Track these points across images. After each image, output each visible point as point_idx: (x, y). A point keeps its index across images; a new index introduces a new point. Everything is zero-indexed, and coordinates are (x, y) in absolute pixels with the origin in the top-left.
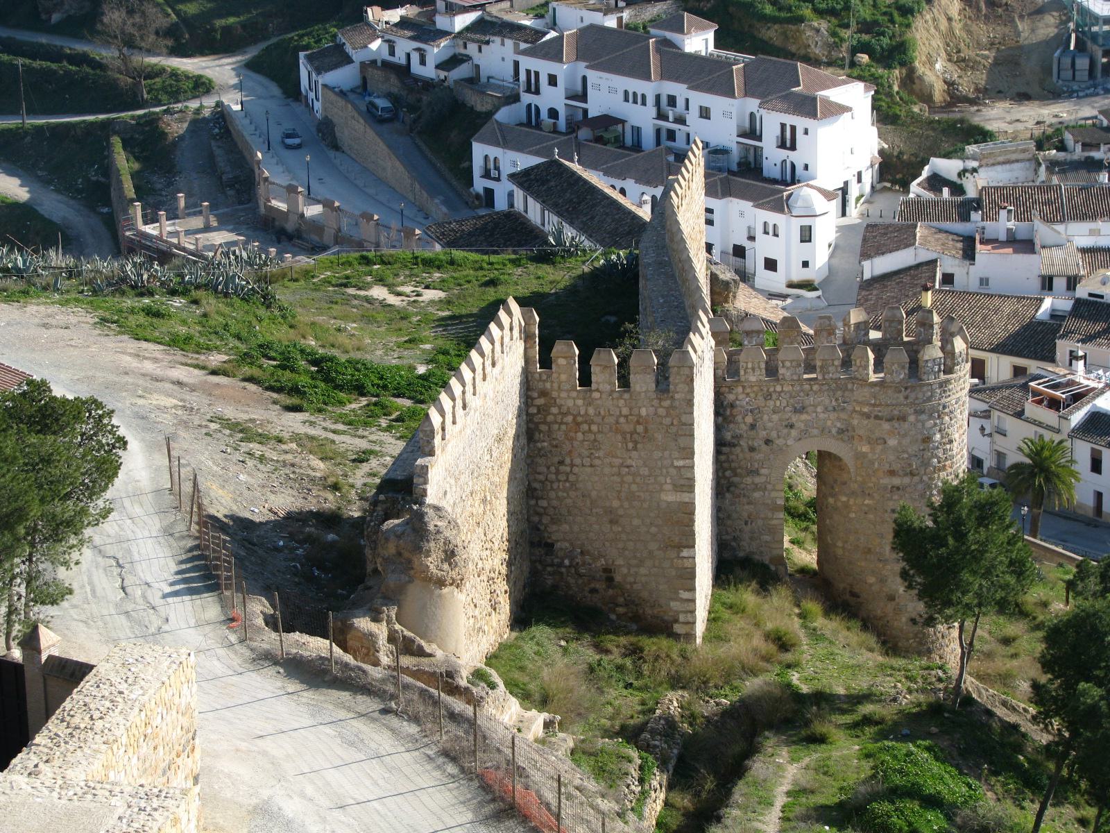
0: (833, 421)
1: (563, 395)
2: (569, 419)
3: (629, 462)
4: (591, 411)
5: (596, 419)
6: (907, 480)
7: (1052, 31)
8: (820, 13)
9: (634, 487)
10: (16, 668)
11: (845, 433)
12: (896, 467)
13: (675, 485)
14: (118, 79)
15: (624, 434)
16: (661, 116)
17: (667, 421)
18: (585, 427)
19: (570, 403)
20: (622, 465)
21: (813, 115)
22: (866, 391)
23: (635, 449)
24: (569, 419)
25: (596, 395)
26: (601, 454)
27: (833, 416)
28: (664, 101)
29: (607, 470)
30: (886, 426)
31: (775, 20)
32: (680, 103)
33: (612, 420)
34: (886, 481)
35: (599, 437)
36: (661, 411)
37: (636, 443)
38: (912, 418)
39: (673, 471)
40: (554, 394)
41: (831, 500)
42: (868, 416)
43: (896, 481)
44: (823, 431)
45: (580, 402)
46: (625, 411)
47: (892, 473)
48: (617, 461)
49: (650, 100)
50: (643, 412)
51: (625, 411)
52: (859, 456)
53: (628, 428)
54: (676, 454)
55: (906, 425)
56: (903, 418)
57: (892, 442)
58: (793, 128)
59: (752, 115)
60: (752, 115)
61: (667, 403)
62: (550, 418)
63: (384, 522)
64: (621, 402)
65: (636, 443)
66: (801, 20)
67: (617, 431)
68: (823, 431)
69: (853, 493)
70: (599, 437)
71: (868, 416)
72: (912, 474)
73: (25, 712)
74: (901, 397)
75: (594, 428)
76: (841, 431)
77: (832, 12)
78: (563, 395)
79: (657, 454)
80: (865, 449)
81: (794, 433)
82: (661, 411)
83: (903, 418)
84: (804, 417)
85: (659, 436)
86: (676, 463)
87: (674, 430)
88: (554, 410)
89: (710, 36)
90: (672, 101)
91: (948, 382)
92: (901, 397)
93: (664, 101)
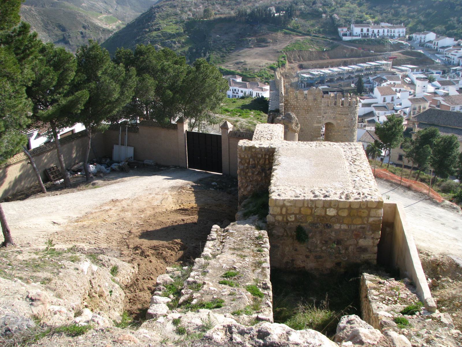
0: (332, 116)
1: (291, 101)
2: (293, 107)
3: (306, 117)
4: (298, 105)
5: (299, 107)
6: (348, 128)
7: (297, 80)
8: (258, 76)
9: (307, 123)
10: (217, 138)
11: (334, 118)
12: (346, 125)
13: (317, 122)
14: (161, 46)
15: (305, 110)
16: (233, 93)
17: (315, 106)
18: (296, 108)
19: (293, 103)
20: (305, 118)
21: (262, 90)
22: (340, 109)
23: (308, 113)
24: (293, 107)
25: (299, 101)
26: (300, 115)
27: (332, 114)
28: (234, 90)
29: (301, 119)
30: (344, 116)
31: (250, 78)
32: (237, 90)
33: (303, 107)
34: (343, 129)
35: (299, 111)
36: (314, 104)
37: (308, 112)
38: (349, 114)
39: (317, 119)
40: (289, 101)
41: (330, 134)
42: (340, 114)
43: (346, 129)
44: (330, 118)
45: (295, 102)
46: (306, 104)
47: (345, 127)
48: (304, 117)
49: (231, 90)
50: (310, 104)
51: (306, 104)
52: (337, 123)
53: (306, 108)
54: (317, 115)
55: (348, 116)
56: (347, 115)
57: (345, 120)
58: (259, 93)
59: (251, 92)
60: (251, 92)
61: (316, 102)
62: (288, 106)
63: (242, 138)
64: (305, 102)
65: (308, 112)
66: (255, 77)
67: (304, 109)
68: (330, 118)
69: (336, 132)
70: (299, 111)
71: (340, 114)
72: (349, 127)
73: (221, 151)
74: (347, 110)
75: (298, 109)
76: (334, 118)
77: (260, 76)
78: (291, 101)
79: (313, 115)
80: (339, 122)
81: (324, 118)
82: (314, 104)
83: (347, 115)
84: (326, 115)
85: (314, 110)
86: (317, 117)
87: (317, 108)
88: (289, 104)
89: (241, 79)
90: (235, 90)
91: (356, 107)
92: (347, 110)
93: (234, 90)
